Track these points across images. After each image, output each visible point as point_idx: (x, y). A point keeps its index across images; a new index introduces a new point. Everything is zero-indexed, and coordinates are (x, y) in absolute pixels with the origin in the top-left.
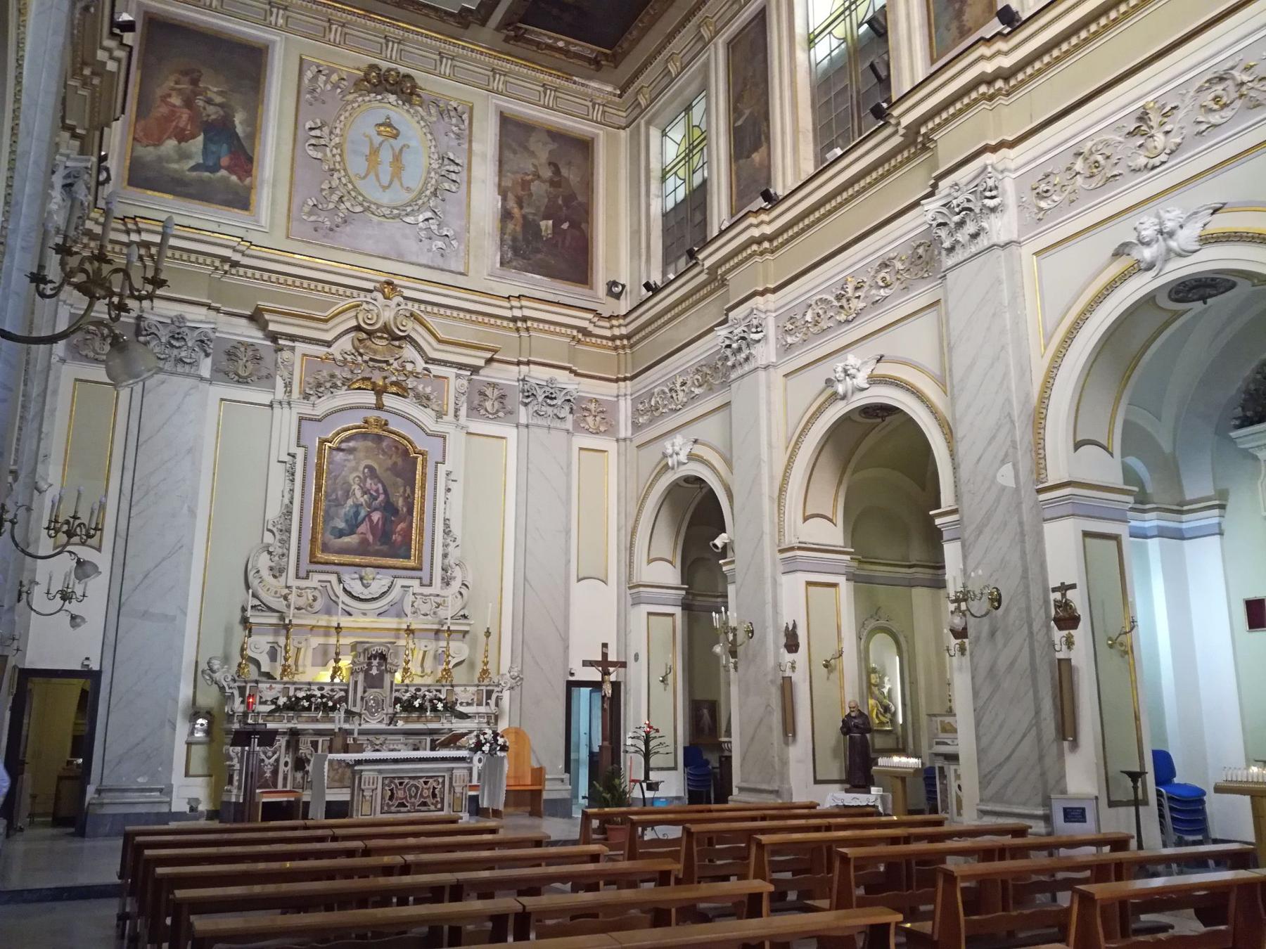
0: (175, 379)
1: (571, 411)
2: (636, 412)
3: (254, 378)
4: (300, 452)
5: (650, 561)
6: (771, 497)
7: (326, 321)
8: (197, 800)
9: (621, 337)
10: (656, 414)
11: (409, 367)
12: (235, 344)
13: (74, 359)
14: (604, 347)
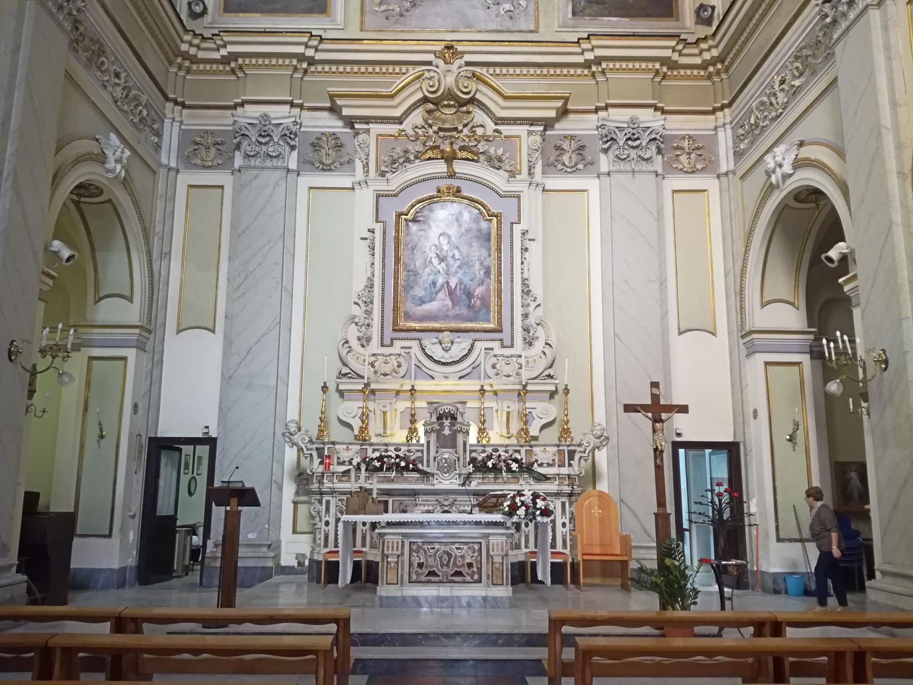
0: (266, 173)
1: (659, 151)
2: (738, 139)
3: (337, 165)
4: (378, 228)
5: (763, 305)
6: (900, 174)
7: (392, 97)
8: (303, 555)
9: (714, 61)
10: (757, 132)
11: (479, 131)
12: (319, 135)
13: (187, 168)
14: (696, 78)
